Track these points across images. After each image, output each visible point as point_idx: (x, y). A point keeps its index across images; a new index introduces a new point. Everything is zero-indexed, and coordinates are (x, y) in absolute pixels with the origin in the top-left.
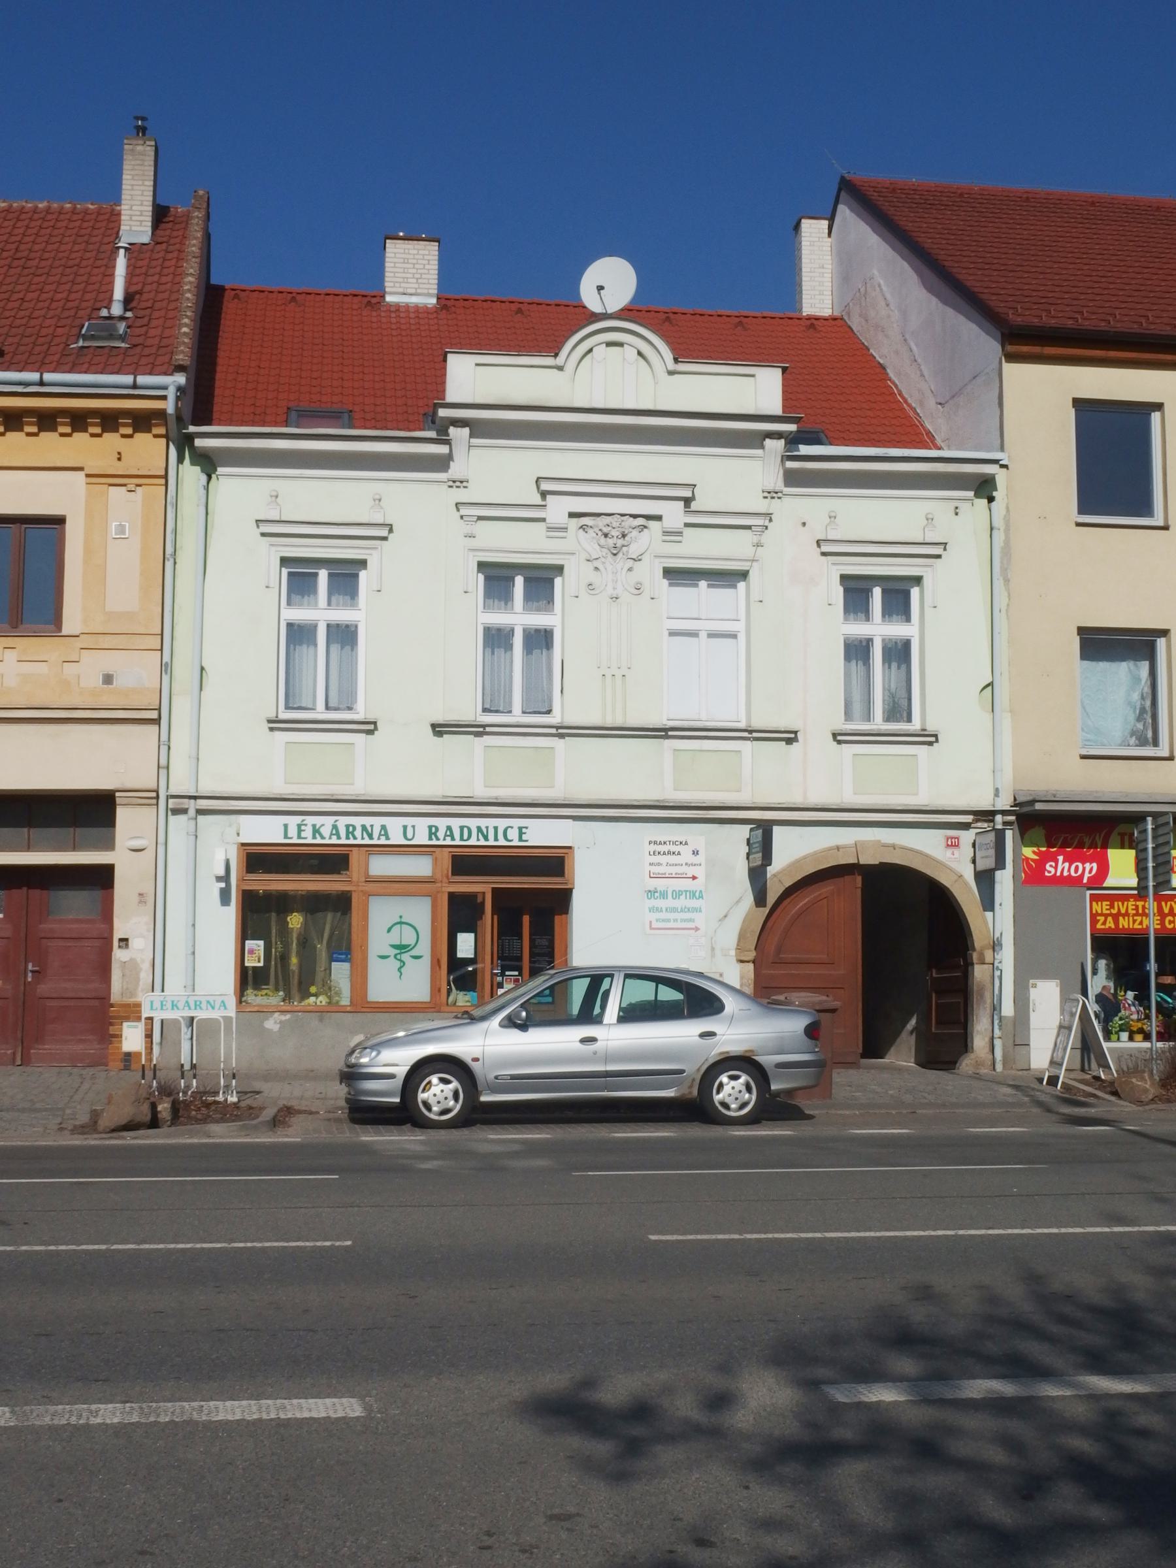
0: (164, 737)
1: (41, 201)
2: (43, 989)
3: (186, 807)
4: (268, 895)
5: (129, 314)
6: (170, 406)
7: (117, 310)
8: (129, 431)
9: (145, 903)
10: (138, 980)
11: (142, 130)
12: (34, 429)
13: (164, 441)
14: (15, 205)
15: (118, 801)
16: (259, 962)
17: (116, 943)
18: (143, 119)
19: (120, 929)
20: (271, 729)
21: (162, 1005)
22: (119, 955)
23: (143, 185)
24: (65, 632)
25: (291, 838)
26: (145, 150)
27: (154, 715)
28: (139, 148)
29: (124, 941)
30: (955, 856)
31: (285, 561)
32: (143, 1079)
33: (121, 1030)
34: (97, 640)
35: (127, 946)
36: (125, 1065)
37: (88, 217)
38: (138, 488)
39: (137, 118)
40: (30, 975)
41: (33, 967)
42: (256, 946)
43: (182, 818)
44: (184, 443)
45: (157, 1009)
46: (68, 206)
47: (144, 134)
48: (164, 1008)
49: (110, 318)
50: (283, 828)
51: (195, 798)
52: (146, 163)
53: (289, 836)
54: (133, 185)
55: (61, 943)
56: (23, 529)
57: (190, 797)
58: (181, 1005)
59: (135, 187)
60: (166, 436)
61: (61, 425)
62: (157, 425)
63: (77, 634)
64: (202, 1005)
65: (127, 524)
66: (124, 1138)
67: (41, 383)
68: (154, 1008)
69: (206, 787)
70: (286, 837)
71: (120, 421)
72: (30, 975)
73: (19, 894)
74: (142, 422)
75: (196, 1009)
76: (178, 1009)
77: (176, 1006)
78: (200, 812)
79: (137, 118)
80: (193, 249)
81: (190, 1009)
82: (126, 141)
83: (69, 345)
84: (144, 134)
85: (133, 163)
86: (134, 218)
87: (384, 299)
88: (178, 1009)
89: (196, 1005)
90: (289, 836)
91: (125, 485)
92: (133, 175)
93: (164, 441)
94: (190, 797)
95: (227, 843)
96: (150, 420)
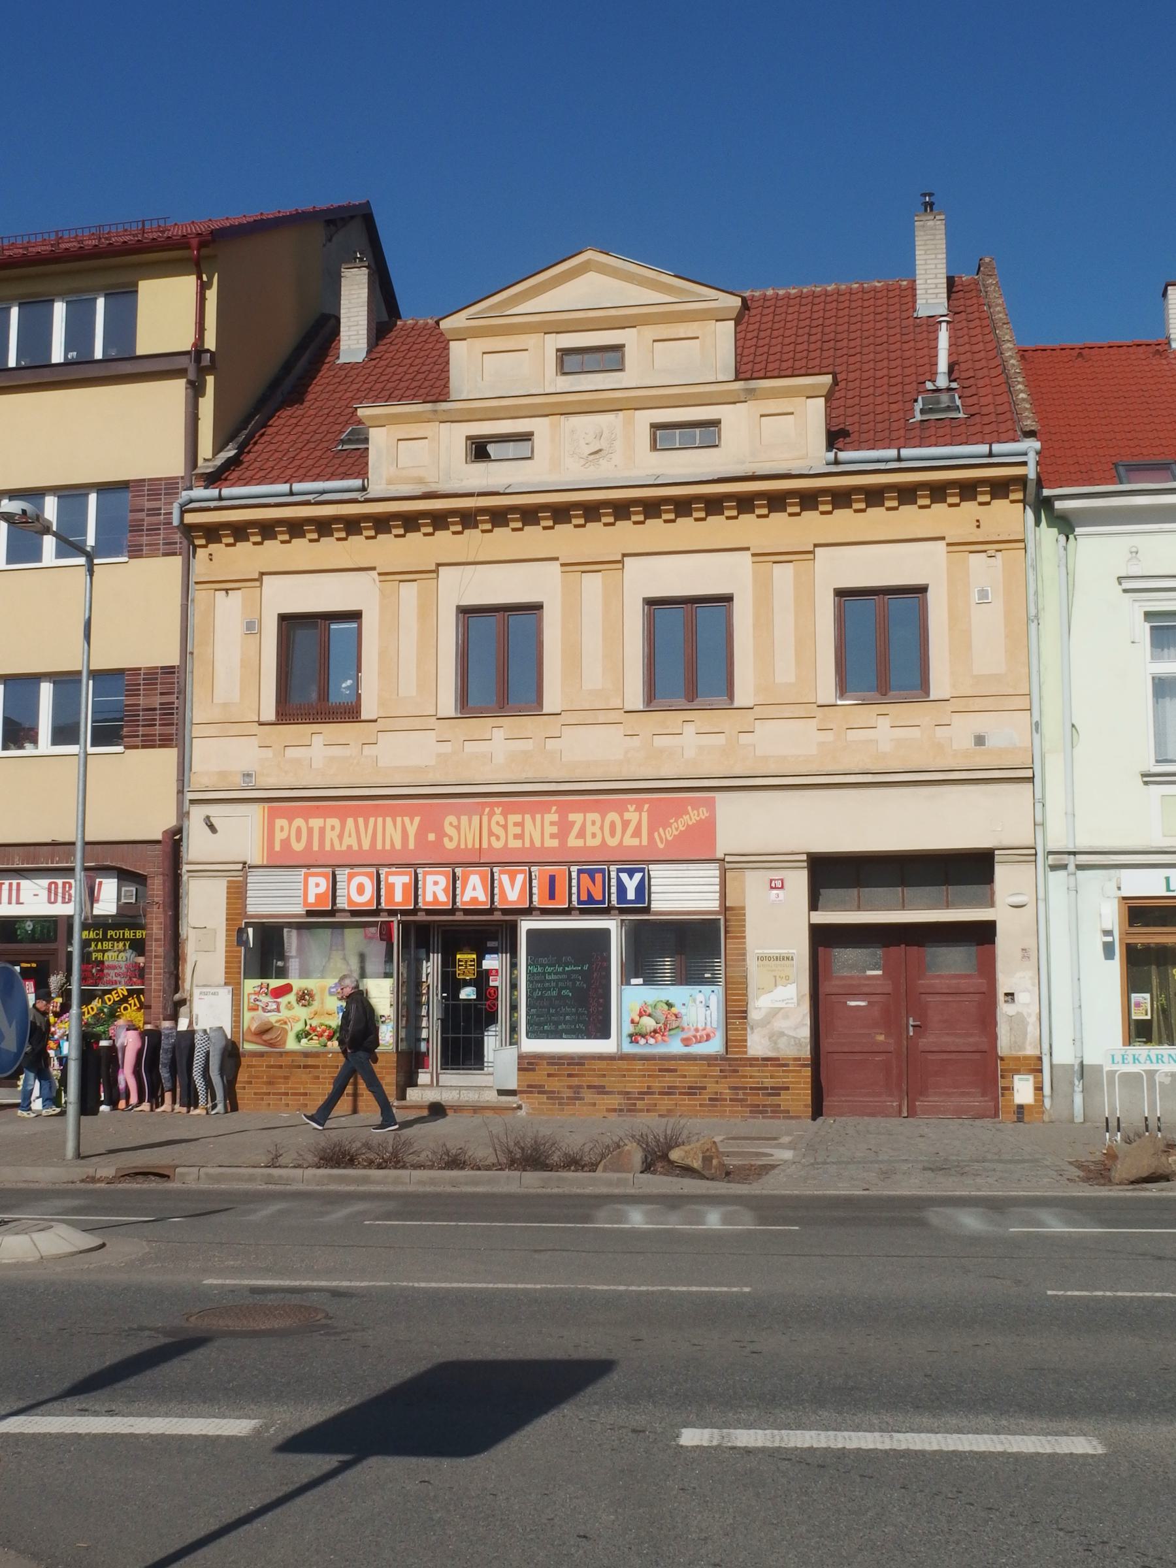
0: (1038, 795)
1: (829, 284)
2: (928, 1041)
3: (1066, 863)
4: (1147, 948)
5: (954, 385)
6: (1031, 472)
7: (942, 382)
8: (765, 511)
9: (1029, 958)
10: (1025, 1034)
11: (929, 207)
12: (862, 506)
13: (1021, 505)
14: (805, 290)
15: (997, 859)
16: (1147, 1015)
17: (1001, 997)
18: (930, 195)
19: (1004, 984)
20: (1146, 783)
21: (1123, 1059)
22: (1004, 1009)
23: (936, 258)
24: (737, 703)
25: (1174, 891)
26: (935, 225)
27: (1028, 774)
28: (930, 223)
29: (1010, 995)
30: (779, 899)
31: (1148, 615)
32: (1147, 1131)
33: (1012, 1082)
34: (965, 703)
35: (1013, 1000)
36: (1018, 1118)
37: (768, 304)
38: (997, 553)
39: (924, 195)
40: (911, 1029)
41: (914, 1021)
42: (1143, 999)
43: (1062, 874)
44: (1043, 506)
45: (1118, 1063)
46: (856, 286)
47: (931, 210)
48: (1126, 1061)
49: (938, 390)
50: (1165, 880)
51: (1074, 853)
52: (938, 237)
53: (1172, 889)
54: (926, 260)
55: (938, 998)
56: (694, 609)
57: (1069, 853)
58: (1142, 1059)
59: (929, 262)
60: (1024, 501)
61: (394, 528)
62: (1014, 491)
63: (751, 706)
64: (1163, 1059)
65: (989, 588)
66: (1146, 1190)
67: (220, 498)
68: (1115, 1062)
69: (1083, 843)
70: (1168, 889)
71: (362, 525)
72: (911, 1029)
73: (899, 951)
74: (1000, 488)
75: (1158, 1062)
76: (1140, 1062)
77: (1138, 1059)
78: (1080, 867)
79: (924, 195)
80: (1001, 315)
81: (1152, 1062)
82: (916, 218)
83: (908, 420)
84: (931, 210)
85: (925, 238)
86: (929, 291)
87: (1170, 346)
88: (1140, 1062)
89: (1157, 1059)
90: (1172, 889)
91: (985, 551)
92: (926, 250)
93: (1021, 505)
94: (1069, 853)
95: (1108, 897)
96: (884, 494)
